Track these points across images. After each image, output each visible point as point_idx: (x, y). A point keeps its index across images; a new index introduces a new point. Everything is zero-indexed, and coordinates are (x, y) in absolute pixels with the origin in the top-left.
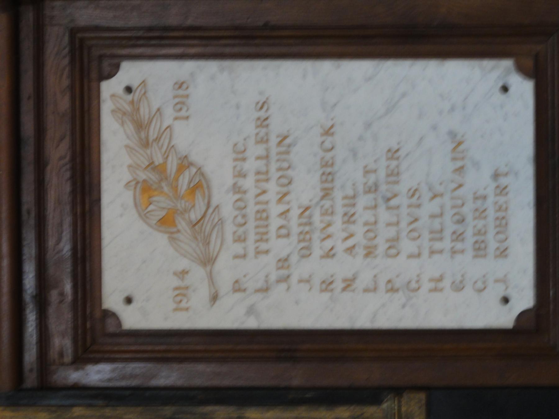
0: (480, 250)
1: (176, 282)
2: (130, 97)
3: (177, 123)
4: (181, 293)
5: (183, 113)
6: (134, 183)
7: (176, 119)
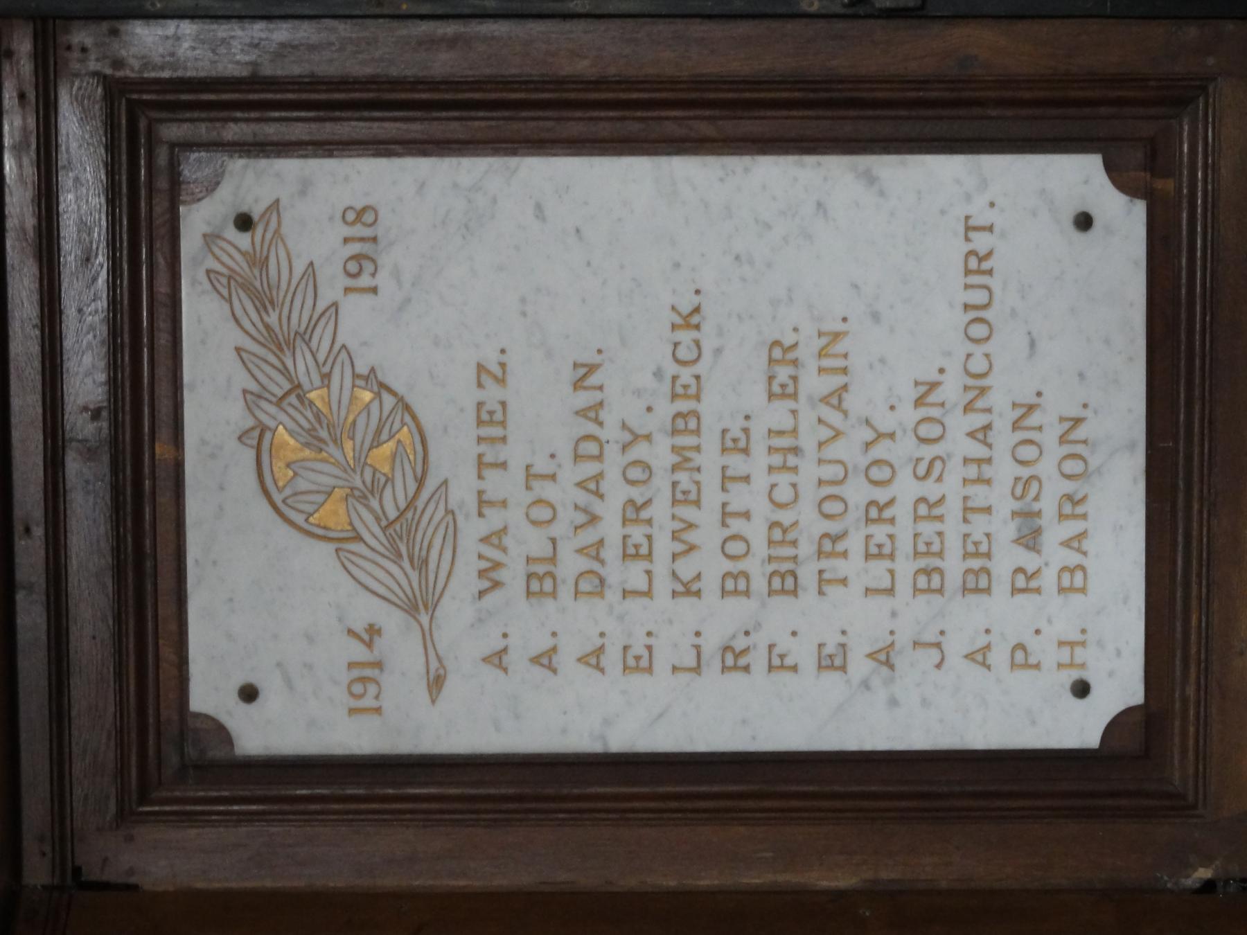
0: (929, 580)
1: (358, 652)
2: (243, 240)
3: (353, 297)
4: (366, 676)
5: (365, 281)
6: (256, 433)
7: (347, 290)
